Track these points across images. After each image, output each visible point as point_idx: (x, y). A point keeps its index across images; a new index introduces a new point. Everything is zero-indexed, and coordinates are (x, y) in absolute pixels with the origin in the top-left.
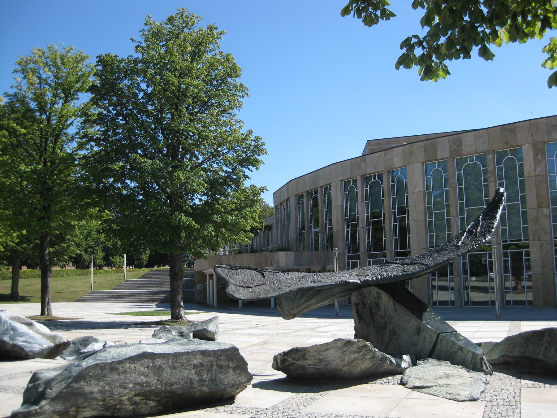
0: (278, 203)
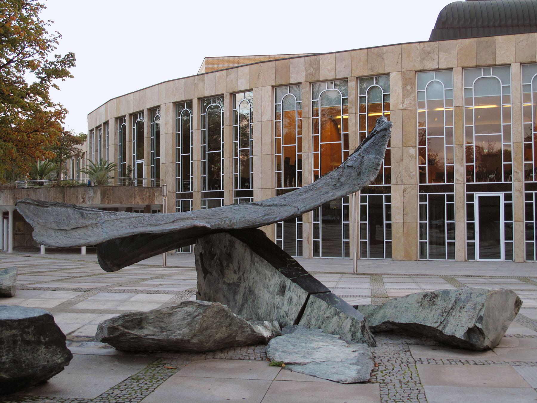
0: (94, 127)
